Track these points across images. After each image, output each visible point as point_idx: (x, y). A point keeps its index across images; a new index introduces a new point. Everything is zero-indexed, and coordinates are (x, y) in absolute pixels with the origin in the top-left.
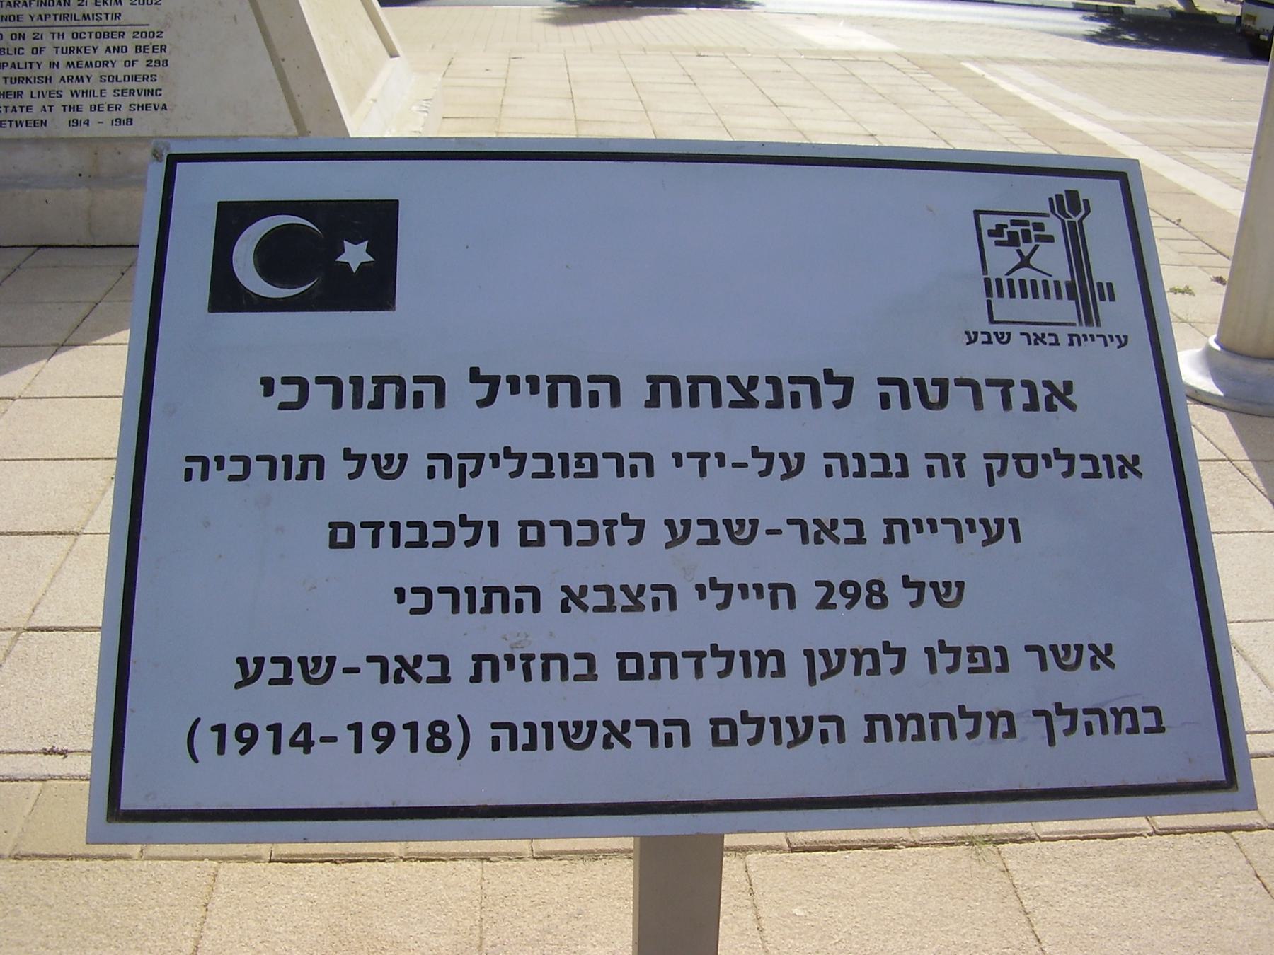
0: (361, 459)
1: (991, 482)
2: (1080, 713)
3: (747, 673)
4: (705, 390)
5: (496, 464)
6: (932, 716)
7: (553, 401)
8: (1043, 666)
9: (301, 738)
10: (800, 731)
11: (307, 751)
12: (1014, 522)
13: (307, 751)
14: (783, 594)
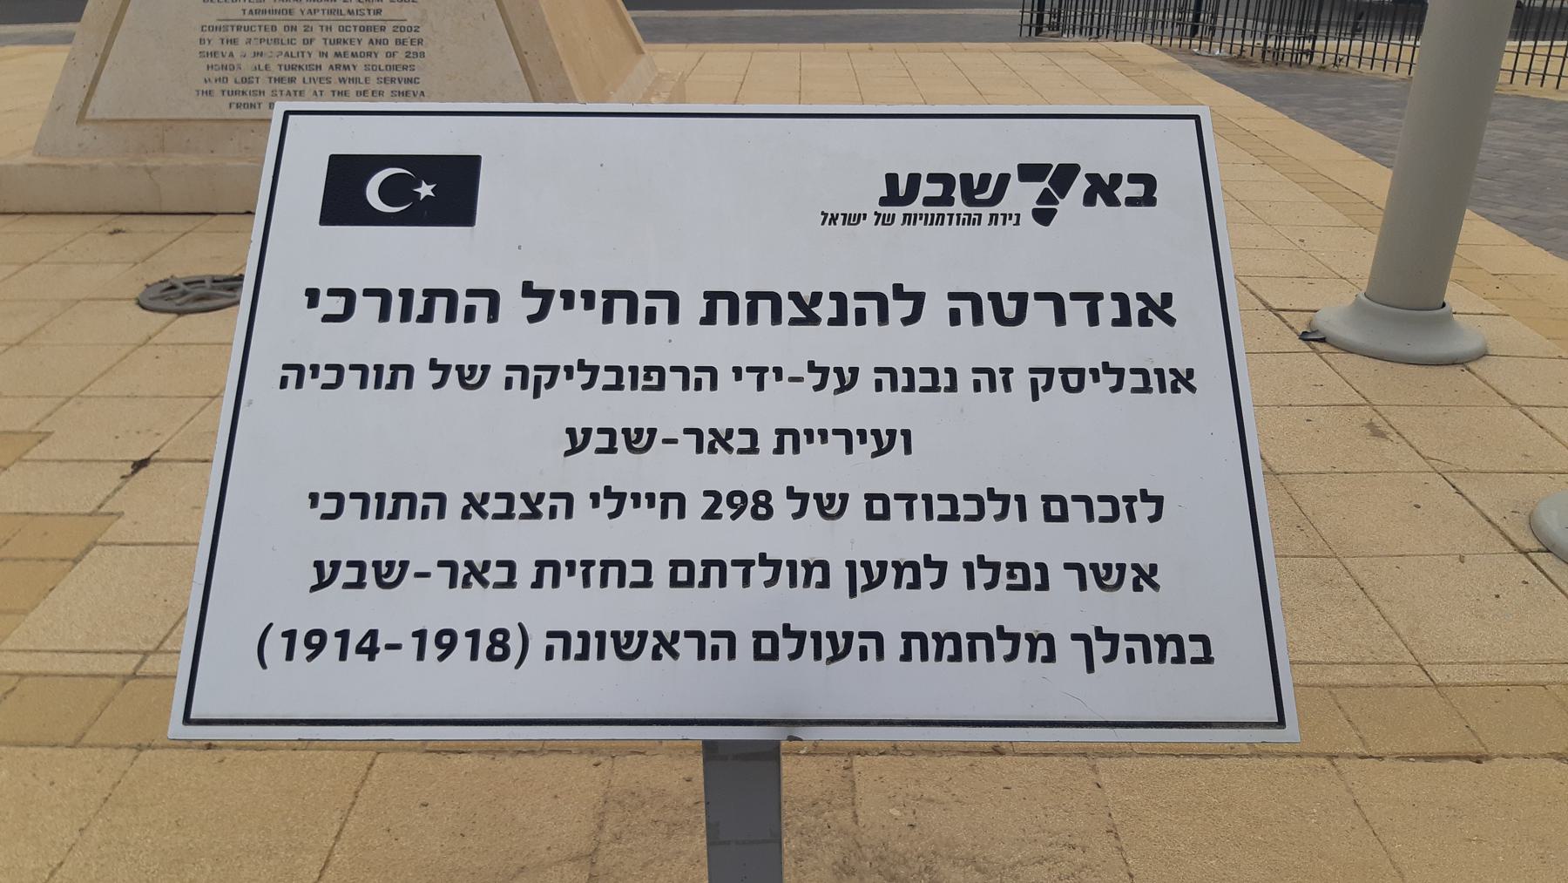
0: (446, 369)
1: (1035, 397)
2: (1122, 639)
3: (793, 583)
4: (764, 306)
5: (569, 376)
6: (969, 636)
7: (608, 317)
8: (1083, 586)
9: (367, 644)
10: (839, 646)
11: (371, 658)
12: (907, 434)
13: (371, 658)
14: (673, 504)
